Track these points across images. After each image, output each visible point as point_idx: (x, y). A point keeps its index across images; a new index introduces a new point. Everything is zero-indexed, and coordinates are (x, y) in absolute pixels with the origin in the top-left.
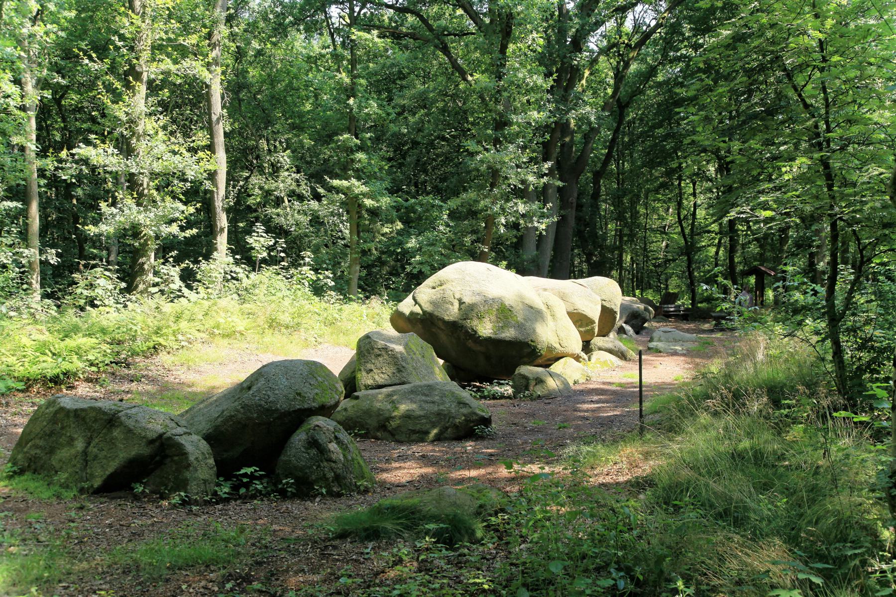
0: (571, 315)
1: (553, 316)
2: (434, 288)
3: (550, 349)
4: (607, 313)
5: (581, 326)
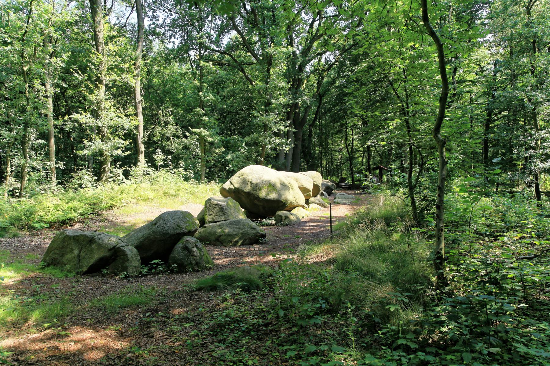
0: (300, 188)
4: (316, 187)
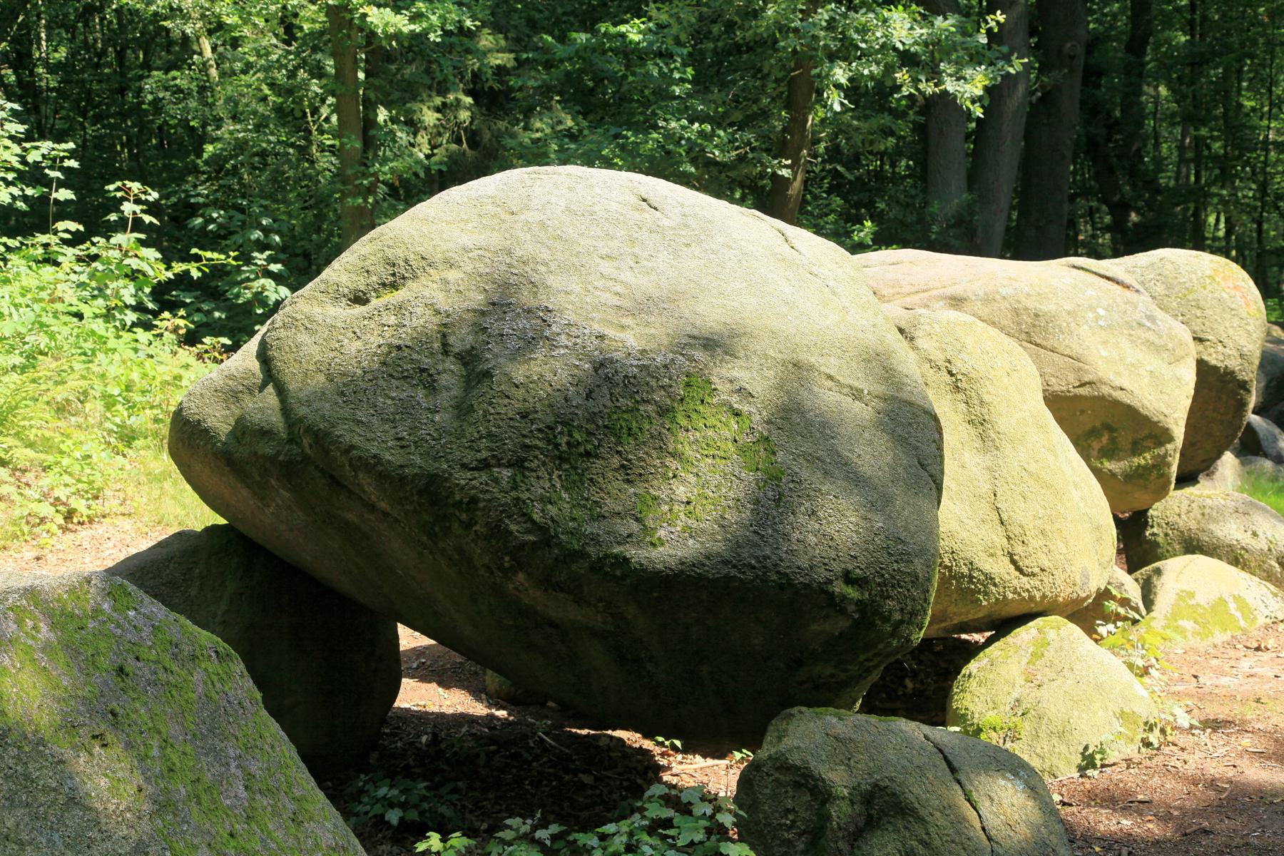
0: (1064, 406)
1: (980, 423)
2: (359, 299)
3: (965, 584)
4: (1214, 385)
5: (1110, 452)
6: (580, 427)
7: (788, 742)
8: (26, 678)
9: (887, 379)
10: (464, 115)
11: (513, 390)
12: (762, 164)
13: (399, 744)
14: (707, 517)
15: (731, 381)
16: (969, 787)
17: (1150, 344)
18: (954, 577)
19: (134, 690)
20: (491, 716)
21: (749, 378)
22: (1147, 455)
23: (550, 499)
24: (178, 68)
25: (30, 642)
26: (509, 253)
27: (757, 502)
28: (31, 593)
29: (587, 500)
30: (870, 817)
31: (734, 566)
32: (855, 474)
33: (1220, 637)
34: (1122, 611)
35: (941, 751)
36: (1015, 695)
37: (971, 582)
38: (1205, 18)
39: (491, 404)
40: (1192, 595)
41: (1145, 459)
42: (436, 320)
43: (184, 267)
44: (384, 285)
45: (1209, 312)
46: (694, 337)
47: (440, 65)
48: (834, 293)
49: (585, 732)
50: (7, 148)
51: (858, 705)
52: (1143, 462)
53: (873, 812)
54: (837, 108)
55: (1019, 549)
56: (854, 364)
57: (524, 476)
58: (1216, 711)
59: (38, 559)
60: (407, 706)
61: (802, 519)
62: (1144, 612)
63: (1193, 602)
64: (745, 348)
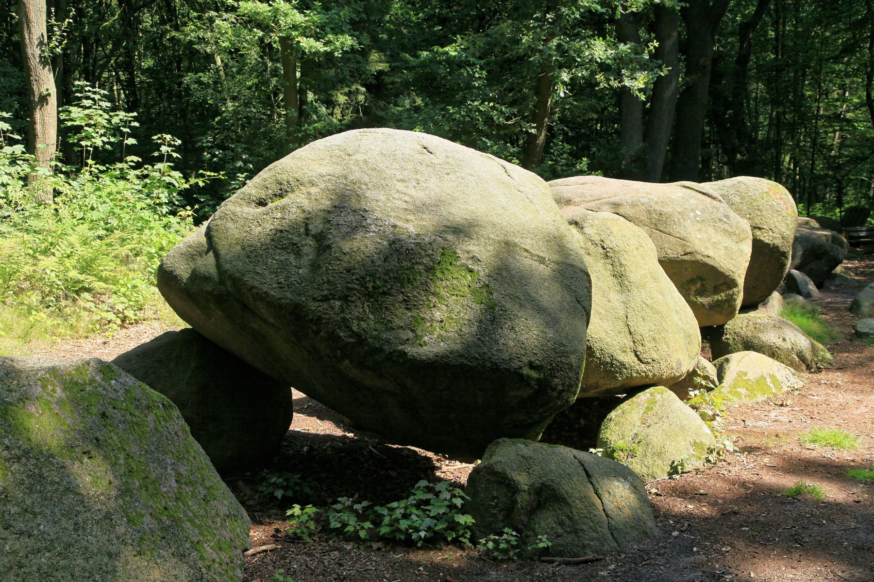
1: (620, 276)
2: (262, 203)
3: (609, 367)
4: (765, 256)
5: (701, 293)
6: (380, 278)
7: (495, 458)
8: (45, 419)
9: (559, 252)
10: (361, 98)
11: (343, 256)
12: (521, 126)
13: (291, 452)
14: (452, 330)
15: (468, 252)
16: (597, 486)
17: (725, 231)
18: (602, 364)
19: (111, 426)
20: (345, 436)
21: (480, 250)
22: (722, 294)
23: (363, 318)
24: (203, 72)
25: (49, 398)
26: (346, 178)
27: (480, 322)
28: (53, 370)
29: (384, 319)
30: (539, 502)
31: (466, 358)
32: (538, 306)
33: (761, 398)
34: (704, 383)
35: (582, 465)
36: (635, 431)
37: (612, 366)
38: (784, 46)
39: (330, 264)
40: (745, 374)
41: (721, 297)
42: (302, 216)
43: (196, 180)
44: (276, 195)
45: (765, 213)
46: (448, 227)
47: (342, 70)
48: (531, 202)
49: (395, 446)
50: (101, 115)
51: (540, 437)
52: (720, 298)
53: (542, 499)
54: (562, 95)
55: (640, 348)
56: (540, 243)
57: (348, 305)
58: (752, 441)
59: (105, 343)
60: (298, 430)
61: (506, 332)
62: (717, 384)
63: (746, 378)
64: (477, 233)
